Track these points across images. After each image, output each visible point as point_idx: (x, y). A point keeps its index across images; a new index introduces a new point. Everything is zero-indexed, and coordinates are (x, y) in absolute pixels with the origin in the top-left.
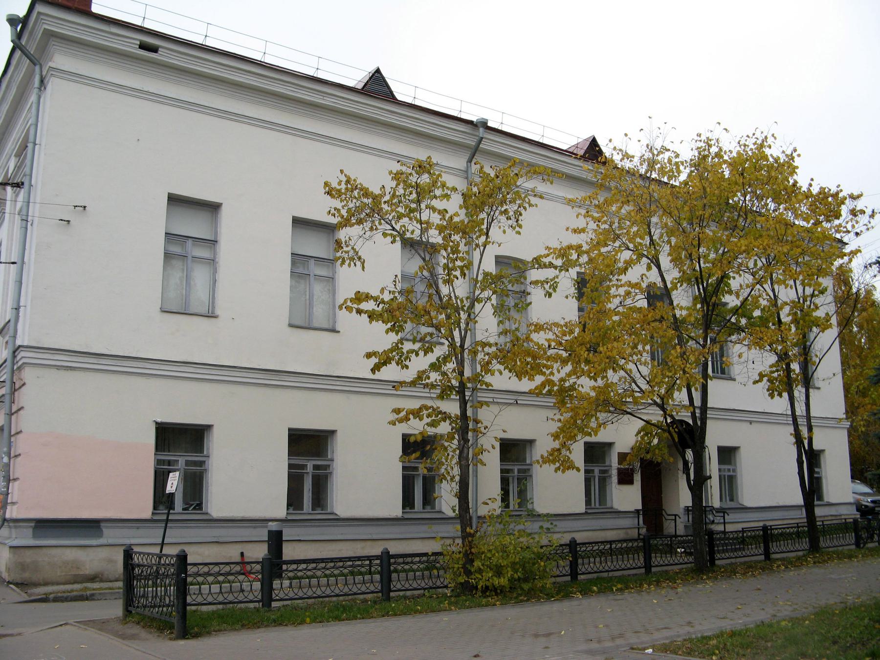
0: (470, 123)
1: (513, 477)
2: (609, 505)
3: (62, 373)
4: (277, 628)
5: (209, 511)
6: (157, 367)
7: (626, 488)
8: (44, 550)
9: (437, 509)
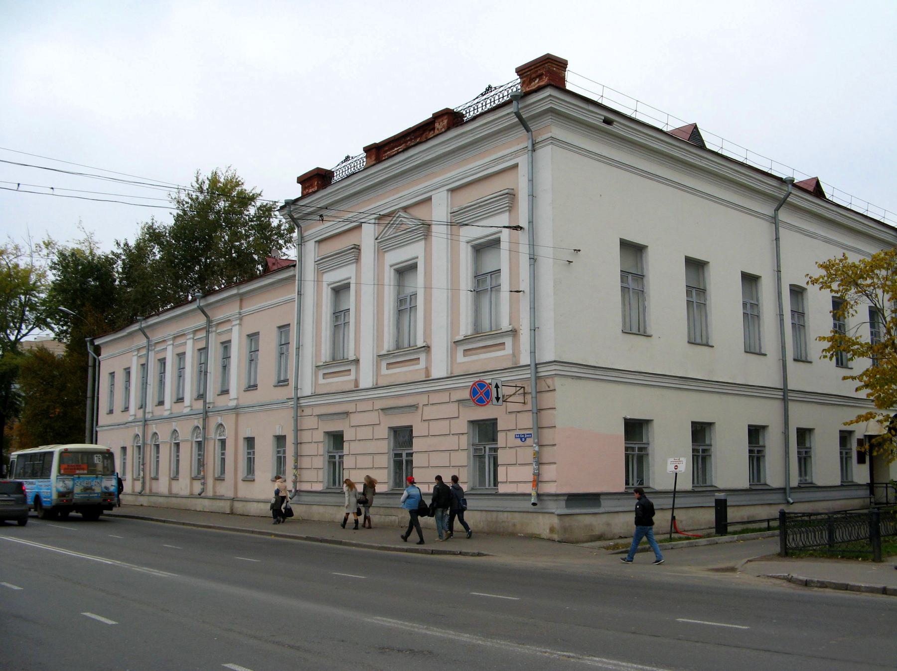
0: (780, 179)
1: (633, 455)
2: (762, 481)
4: (827, 560)
5: (651, 485)
8: (575, 517)
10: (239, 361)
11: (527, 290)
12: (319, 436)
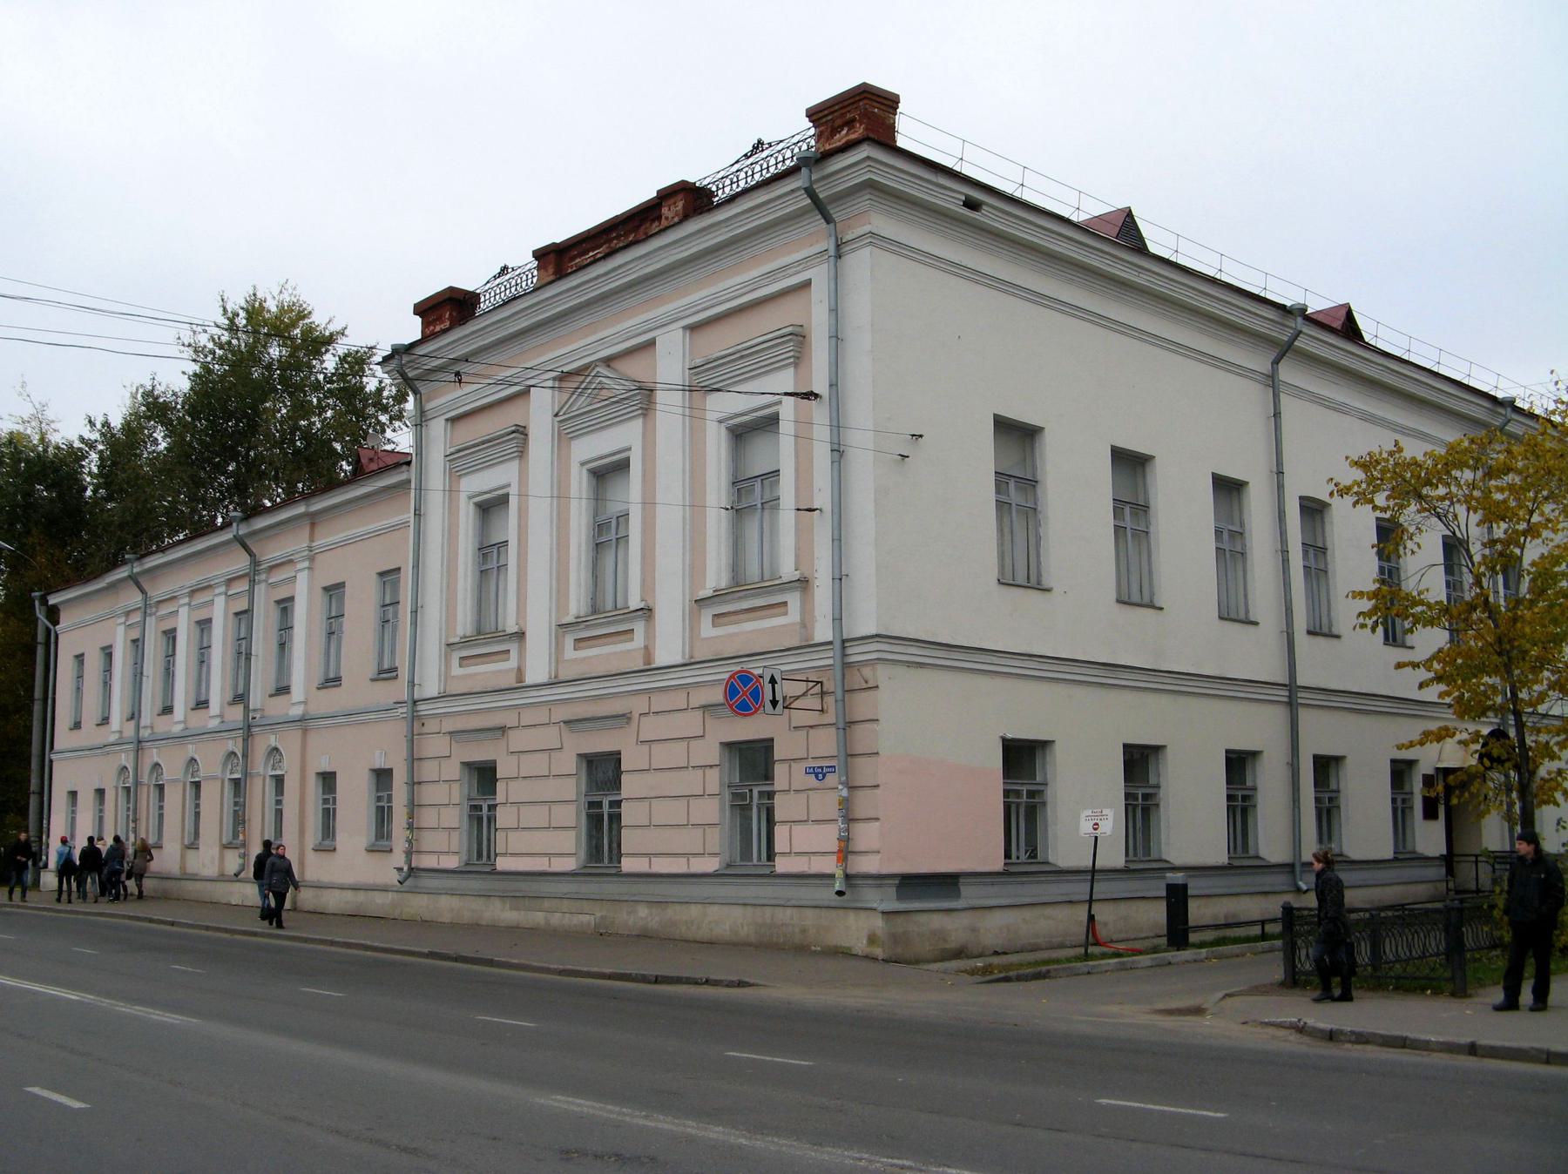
0: (1281, 307)
1: (1018, 805)
3: (912, 671)
5: (1051, 859)
6: (1003, 661)
7: (1431, 824)
9: (1252, 853)
10: (309, 635)
11: (827, 507)
12: (453, 770)
